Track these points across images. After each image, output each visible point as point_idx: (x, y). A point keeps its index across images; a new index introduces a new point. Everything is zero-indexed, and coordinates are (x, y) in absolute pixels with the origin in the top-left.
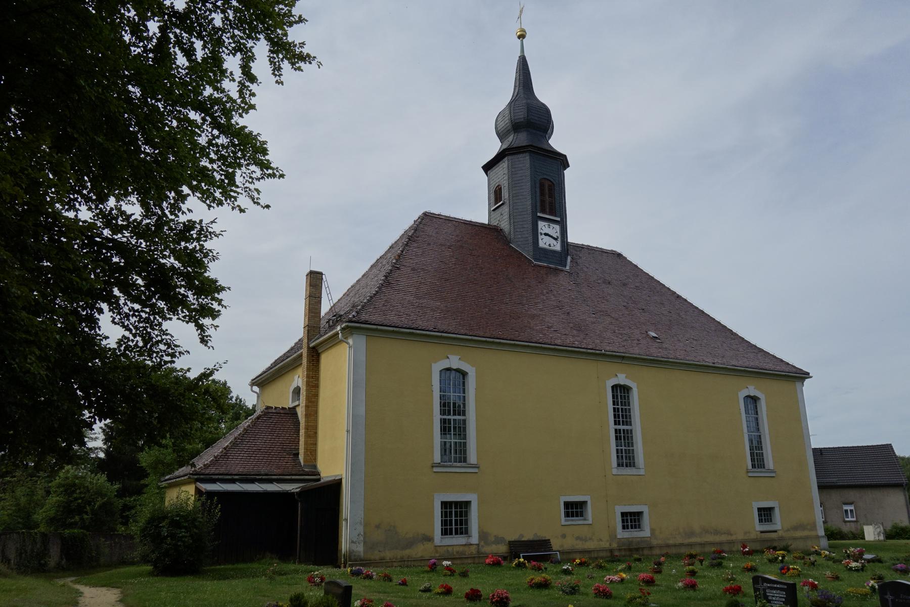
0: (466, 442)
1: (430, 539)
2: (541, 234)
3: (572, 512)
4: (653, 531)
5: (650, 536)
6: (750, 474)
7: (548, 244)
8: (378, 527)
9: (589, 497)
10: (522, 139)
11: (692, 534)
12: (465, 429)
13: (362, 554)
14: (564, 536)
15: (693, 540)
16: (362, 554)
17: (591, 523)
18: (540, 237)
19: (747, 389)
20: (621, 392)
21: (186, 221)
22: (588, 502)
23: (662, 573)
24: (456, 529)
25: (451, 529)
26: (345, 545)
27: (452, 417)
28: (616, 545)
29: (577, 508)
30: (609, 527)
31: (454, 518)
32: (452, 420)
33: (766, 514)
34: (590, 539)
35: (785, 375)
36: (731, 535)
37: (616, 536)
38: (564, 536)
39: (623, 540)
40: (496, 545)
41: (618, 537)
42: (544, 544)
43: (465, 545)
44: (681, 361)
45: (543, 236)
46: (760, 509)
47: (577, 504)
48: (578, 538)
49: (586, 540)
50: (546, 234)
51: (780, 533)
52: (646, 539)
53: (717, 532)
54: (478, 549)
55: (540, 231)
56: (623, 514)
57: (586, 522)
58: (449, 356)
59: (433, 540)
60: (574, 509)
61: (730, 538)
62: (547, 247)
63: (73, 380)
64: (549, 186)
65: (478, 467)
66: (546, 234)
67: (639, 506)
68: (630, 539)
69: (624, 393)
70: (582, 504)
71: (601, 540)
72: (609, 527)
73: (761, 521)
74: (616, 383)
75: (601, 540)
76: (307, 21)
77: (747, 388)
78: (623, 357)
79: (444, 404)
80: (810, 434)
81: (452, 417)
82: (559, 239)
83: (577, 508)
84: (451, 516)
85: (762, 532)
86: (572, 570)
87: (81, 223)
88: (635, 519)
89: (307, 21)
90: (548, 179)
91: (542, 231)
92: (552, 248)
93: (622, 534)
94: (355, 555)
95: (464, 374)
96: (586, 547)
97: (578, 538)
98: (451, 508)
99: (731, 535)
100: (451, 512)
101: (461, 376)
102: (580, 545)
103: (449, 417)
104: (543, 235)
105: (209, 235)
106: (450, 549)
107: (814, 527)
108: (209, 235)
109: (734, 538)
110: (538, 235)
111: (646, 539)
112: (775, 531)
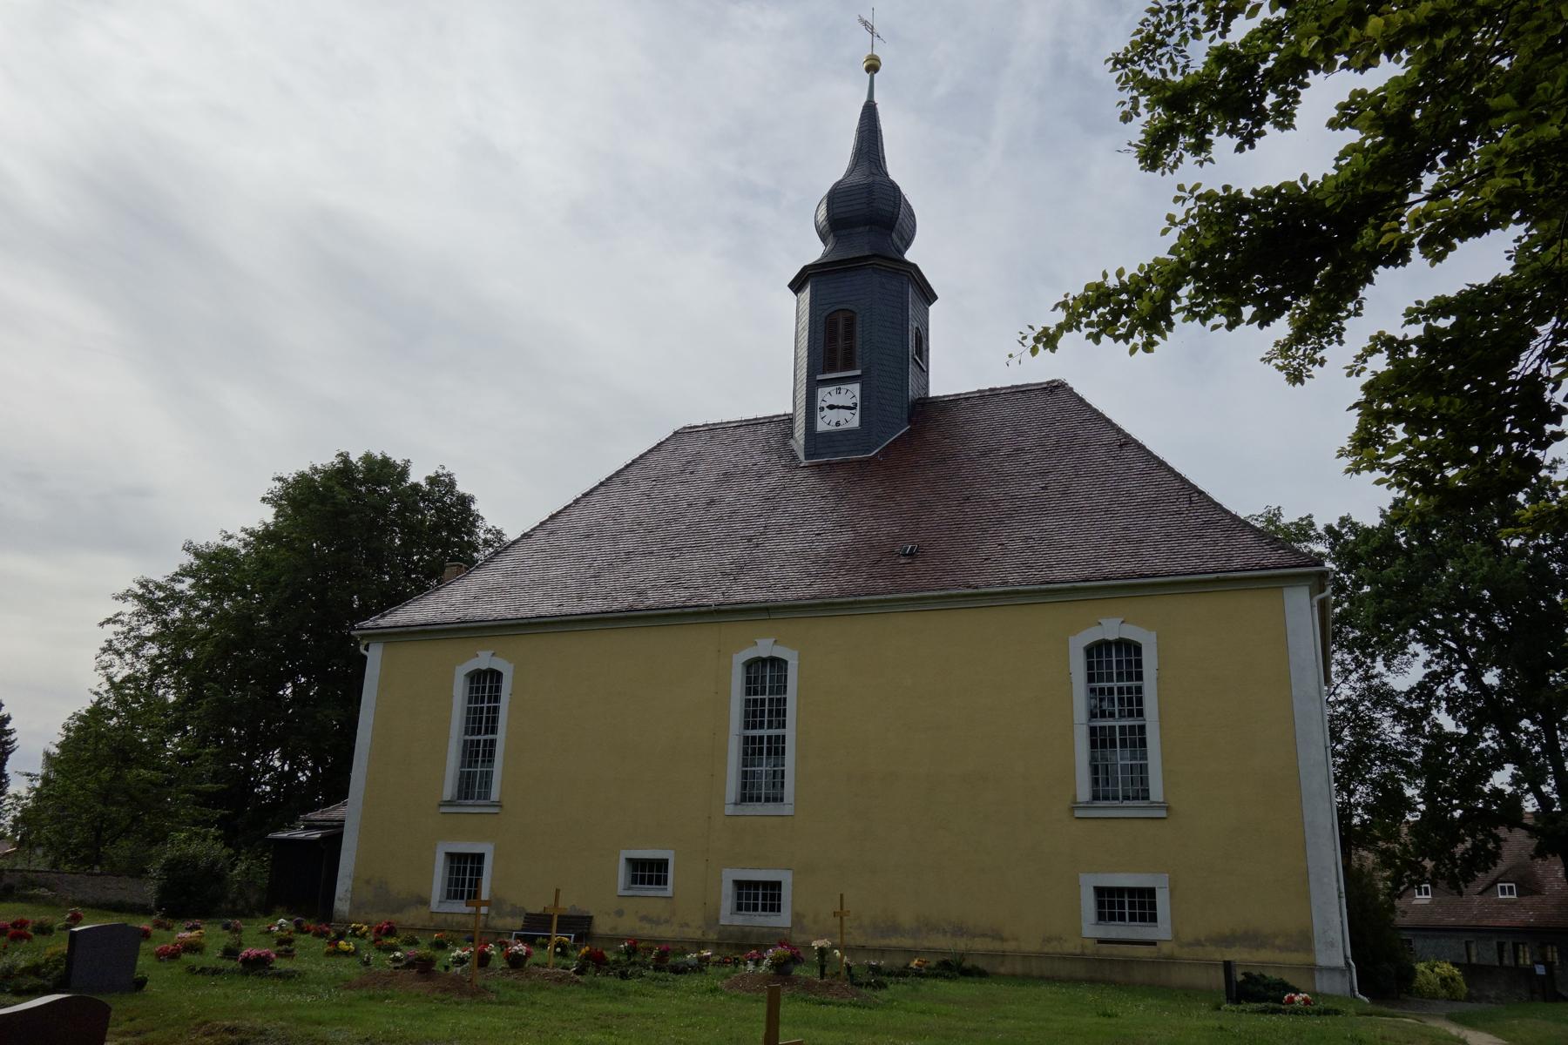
1: (425, 902)
2: (822, 409)
3: (651, 877)
4: (797, 917)
5: (790, 926)
6: (1078, 814)
7: (833, 423)
8: (368, 882)
9: (1167, 875)
10: (859, 247)
11: (895, 929)
12: (745, 753)
13: (347, 914)
14: (620, 913)
15: (894, 942)
16: (347, 914)
17: (671, 895)
19: (1099, 627)
20: (491, 681)
24: (469, 892)
25: (463, 892)
26: (342, 905)
27: (1115, 684)
28: (715, 937)
30: (705, 904)
31: (468, 877)
32: (765, 737)
33: (465, 870)
34: (667, 921)
35: (1218, 580)
36: (1002, 939)
37: (717, 920)
38: (620, 913)
39: (731, 928)
40: (512, 918)
41: (721, 923)
42: (587, 920)
43: (469, 914)
44: (882, 597)
46: (1100, 892)
47: (637, 863)
48: (644, 918)
49: (657, 922)
50: (831, 407)
51: (1166, 949)
52: (780, 930)
53: (959, 931)
54: (487, 921)
56: (740, 885)
57: (660, 894)
58: (1100, 621)
59: (429, 906)
60: (649, 872)
61: (996, 946)
62: (832, 428)
65: (501, 806)
66: (831, 407)
67: (773, 871)
68: (747, 929)
69: (478, 683)
70: (662, 865)
71: (687, 925)
72: (705, 904)
73: (1101, 917)
74: (1099, 637)
75: (687, 925)
77: (1100, 623)
78: (767, 609)
79: (778, 714)
80: (1076, 722)
81: (1115, 684)
82: (858, 408)
84: (465, 874)
85: (1101, 941)
86: (576, 959)
90: (847, 310)
92: (844, 426)
93: (729, 916)
94: (339, 916)
95: (1131, 649)
96: (656, 934)
97: (644, 918)
98: (466, 863)
99: (1002, 939)
100: (465, 869)
102: (647, 930)
103: (479, 737)
104: (826, 409)
106: (449, 918)
107: (1304, 940)
109: (1010, 946)
110: (861, 403)
111: (780, 930)
112: (1153, 943)
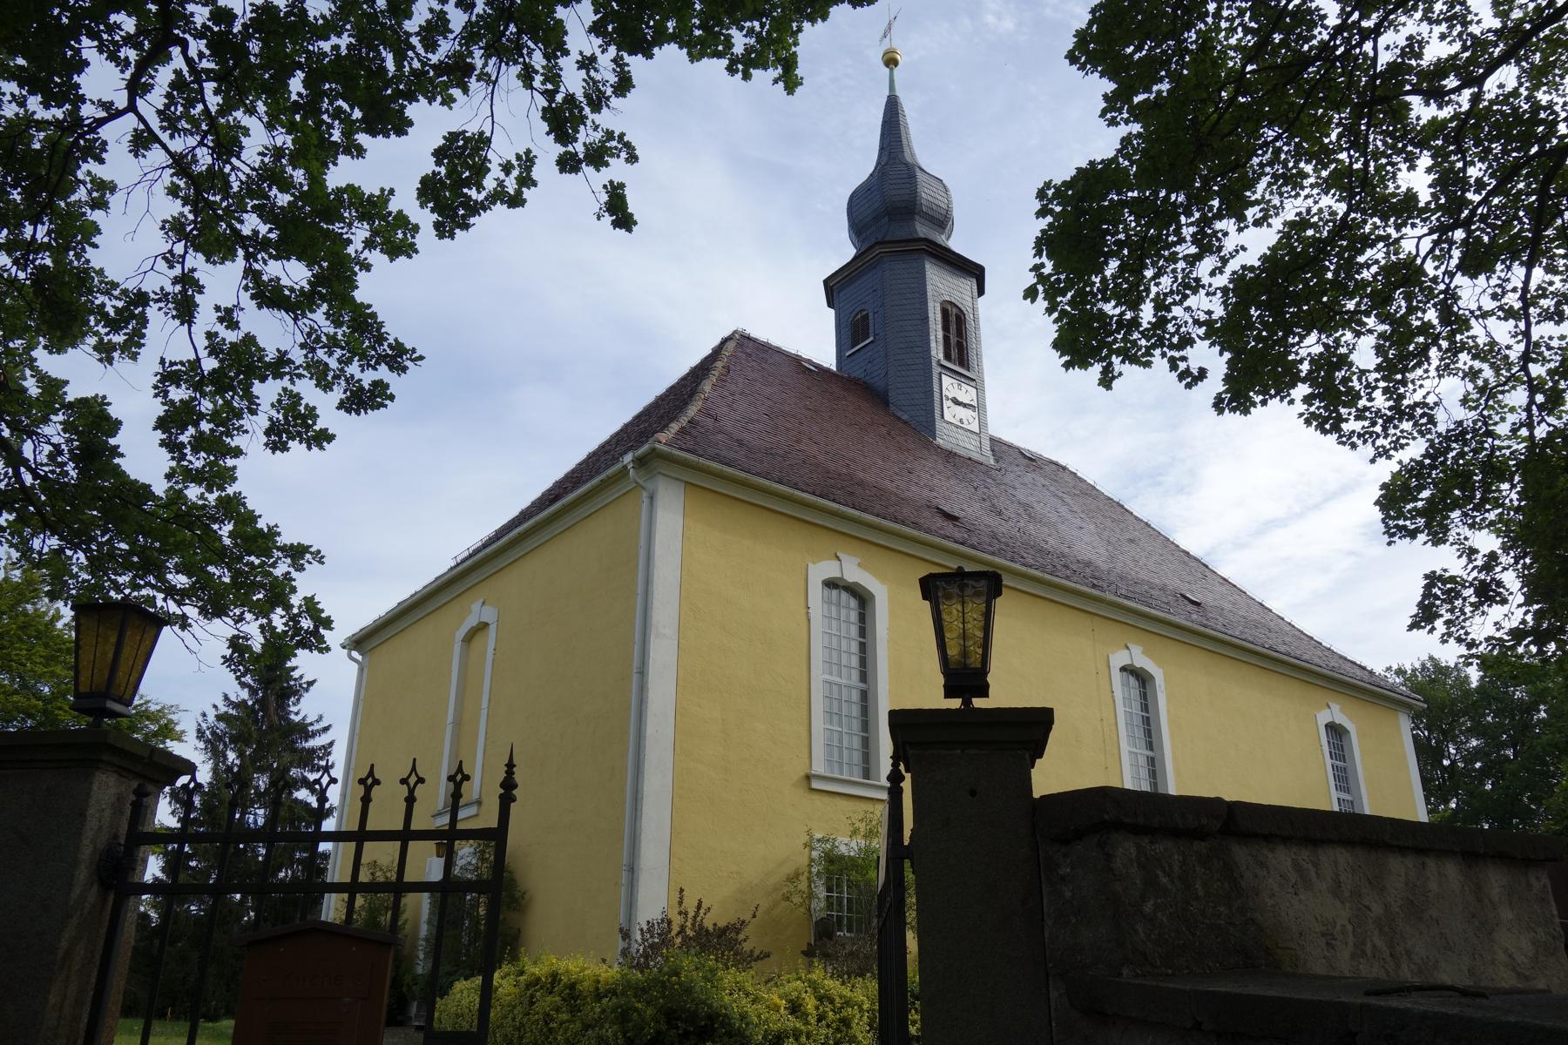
2: (948, 399)
18: (947, 404)
45: (949, 403)
55: (945, 392)
63: (1478, 765)
91: (948, 393)
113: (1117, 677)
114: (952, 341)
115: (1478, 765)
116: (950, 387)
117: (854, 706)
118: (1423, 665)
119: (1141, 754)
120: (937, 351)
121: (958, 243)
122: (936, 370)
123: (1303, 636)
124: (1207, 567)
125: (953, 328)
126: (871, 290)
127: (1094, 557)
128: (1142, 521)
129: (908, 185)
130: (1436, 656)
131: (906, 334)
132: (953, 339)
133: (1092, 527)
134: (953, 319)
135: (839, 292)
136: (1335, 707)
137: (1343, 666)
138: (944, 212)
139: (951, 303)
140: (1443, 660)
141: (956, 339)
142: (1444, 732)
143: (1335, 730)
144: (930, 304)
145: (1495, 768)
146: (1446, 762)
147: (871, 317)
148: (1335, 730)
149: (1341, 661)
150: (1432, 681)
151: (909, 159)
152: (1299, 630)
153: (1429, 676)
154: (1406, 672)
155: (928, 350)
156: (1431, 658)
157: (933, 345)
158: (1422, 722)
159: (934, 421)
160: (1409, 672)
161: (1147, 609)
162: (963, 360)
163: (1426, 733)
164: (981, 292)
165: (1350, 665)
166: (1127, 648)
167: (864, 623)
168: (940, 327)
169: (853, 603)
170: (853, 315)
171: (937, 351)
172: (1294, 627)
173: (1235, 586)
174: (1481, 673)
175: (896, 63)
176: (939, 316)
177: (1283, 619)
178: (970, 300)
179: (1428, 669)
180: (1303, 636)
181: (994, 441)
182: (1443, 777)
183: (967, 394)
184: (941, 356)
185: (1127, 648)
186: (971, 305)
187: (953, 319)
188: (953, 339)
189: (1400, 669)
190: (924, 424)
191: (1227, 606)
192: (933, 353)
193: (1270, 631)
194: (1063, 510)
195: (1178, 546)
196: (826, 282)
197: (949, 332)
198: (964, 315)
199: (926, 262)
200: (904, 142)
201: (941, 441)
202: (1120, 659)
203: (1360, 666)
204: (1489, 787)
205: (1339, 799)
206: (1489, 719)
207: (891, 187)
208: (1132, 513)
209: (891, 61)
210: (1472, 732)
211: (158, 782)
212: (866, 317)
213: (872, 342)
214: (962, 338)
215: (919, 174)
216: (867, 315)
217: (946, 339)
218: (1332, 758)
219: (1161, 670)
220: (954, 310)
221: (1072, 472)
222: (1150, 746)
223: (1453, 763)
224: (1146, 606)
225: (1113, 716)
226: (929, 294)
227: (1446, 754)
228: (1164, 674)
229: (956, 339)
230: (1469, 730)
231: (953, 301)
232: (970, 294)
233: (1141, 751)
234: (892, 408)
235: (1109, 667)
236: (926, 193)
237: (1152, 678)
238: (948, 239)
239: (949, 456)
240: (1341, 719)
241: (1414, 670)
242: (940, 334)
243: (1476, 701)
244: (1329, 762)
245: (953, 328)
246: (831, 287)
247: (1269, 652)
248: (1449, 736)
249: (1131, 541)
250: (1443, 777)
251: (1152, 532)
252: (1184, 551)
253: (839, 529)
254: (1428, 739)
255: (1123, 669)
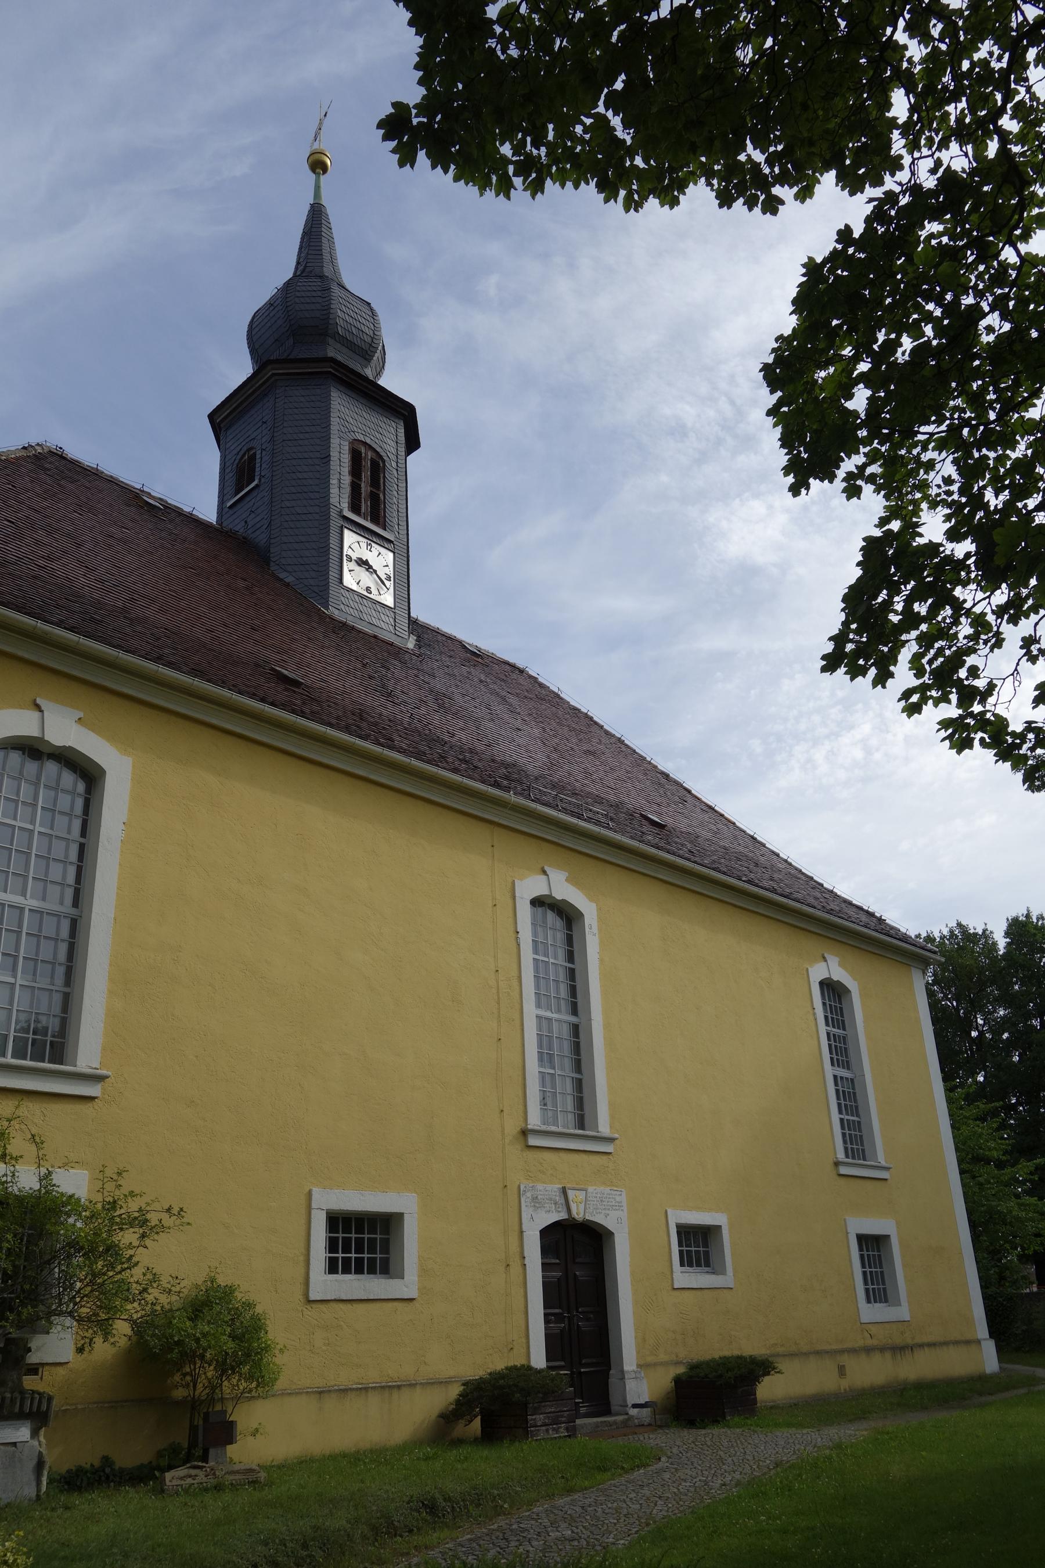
0: (67, 1018)
2: (350, 559)
18: (346, 566)
21: (681, 197)
22: (407, 1220)
23: (33, 1350)
29: (360, 1230)
45: (353, 565)
55: (346, 550)
63: (1005, 1036)
64: (372, 460)
76: (1034, 708)
83: (360, 1230)
87: (1011, 414)
88: (372, 1242)
89: (1034, 708)
91: (350, 552)
101: (81, 787)
105: (857, 638)
108: (857, 638)
113: (525, 912)
114: (363, 490)
115: (1005, 1036)
116: (355, 546)
117: (562, 1002)
118: (951, 932)
119: (559, 1021)
120: (340, 497)
121: (391, 381)
122: (335, 522)
123: (800, 876)
124: (689, 792)
125: (366, 475)
126: (260, 424)
127: (522, 761)
128: (614, 736)
129: (320, 300)
130: (964, 923)
131: (299, 475)
132: (365, 488)
133: (536, 732)
134: (367, 464)
135: (227, 430)
136: (833, 961)
137: (846, 910)
138: (368, 340)
139: (365, 444)
140: (971, 927)
141: (369, 489)
142: (972, 1002)
143: (832, 990)
144: (335, 441)
145: (1022, 1040)
146: (974, 1034)
147: (258, 456)
148: (832, 990)
149: (843, 905)
150: (960, 948)
151: (327, 271)
152: (796, 869)
153: (958, 944)
154: (935, 939)
155: (327, 496)
156: (959, 925)
157: (334, 491)
158: (950, 992)
159: (326, 586)
160: (938, 939)
161: (574, 820)
162: (377, 515)
163: (955, 1004)
164: (413, 443)
165: (854, 910)
166: (544, 872)
167: (87, 816)
168: (346, 470)
169: (559, 923)
170: (239, 457)
171: (340, 497)
172: (790, 864)
173: (722, 815)
174: (1008, 940)
175: (325, 169)
176: (346, 458)
177: (778, 855)
178: (393, 444)
179: (957, 936)
180: (800, 876)
181: (416, 627)
182: (971, 1050)
183: (382, 559)
184: (345, 505)
185: (544, 872)
186: (394, 451)
187: (367, 464)
188: (365, 488)
189: (928, 936)
190: (316, 589)
191: (705, 834)
192: (334, 500)
193: (757, 865)
194: (499, 709)
195: (655, 767)
196: (211, 417)
197: (360, 479)
198: (384, 461)
199: (332, 389)
200: (326, 256)
201: (336, 612)
202: (532, 886)
203: (867, 912)
204: (1016, 1059)
205: (835, 1077)
206: (1017, 987)
207: (297, 300)
208: (602, 727)
209: (318, 166)
210: (999, 1001)
211: (542, 1061)
212: (253, 458)
213: (257, 486)
214: (378, 488)
215: (336, 290)
216: (255, 454)
217: (355, 488)
218: (827, 1024)
219: (594, 906)
220: (370, 454)
221: (531, 677)
222: (575, 1011)
223: (981, 1034)
224: (573, 816)
225: (515, 966)
226: (334, 428)
227: (974, 1024)
228: (599, 909)
229: (369, 489)
230: (996, 1000)
231: (368, 441)
232: (393, 437)
233: (555, 1016)
234: (273, 567)
235: (514, 897)
236: (342, 315)
237: (580, 915)
238: (379, 374)
239: (343, 629)
240: (838, 974)
241: (943, 937)
242: (347, 479)
243: (1004, 968)
244: (823, 1029)
245: (366, 475)
246: (219, 424)
247: (747, 886)
248: (976, 1006)
249: (588, 752)
250: (971, 1050)
251: (624, 749)
252: (663, 773)
253: (43, 661)
254: (957, 1010)
255: (537, 902)
